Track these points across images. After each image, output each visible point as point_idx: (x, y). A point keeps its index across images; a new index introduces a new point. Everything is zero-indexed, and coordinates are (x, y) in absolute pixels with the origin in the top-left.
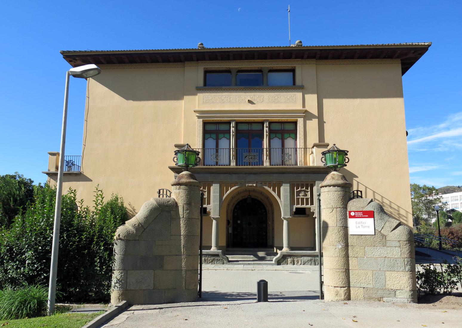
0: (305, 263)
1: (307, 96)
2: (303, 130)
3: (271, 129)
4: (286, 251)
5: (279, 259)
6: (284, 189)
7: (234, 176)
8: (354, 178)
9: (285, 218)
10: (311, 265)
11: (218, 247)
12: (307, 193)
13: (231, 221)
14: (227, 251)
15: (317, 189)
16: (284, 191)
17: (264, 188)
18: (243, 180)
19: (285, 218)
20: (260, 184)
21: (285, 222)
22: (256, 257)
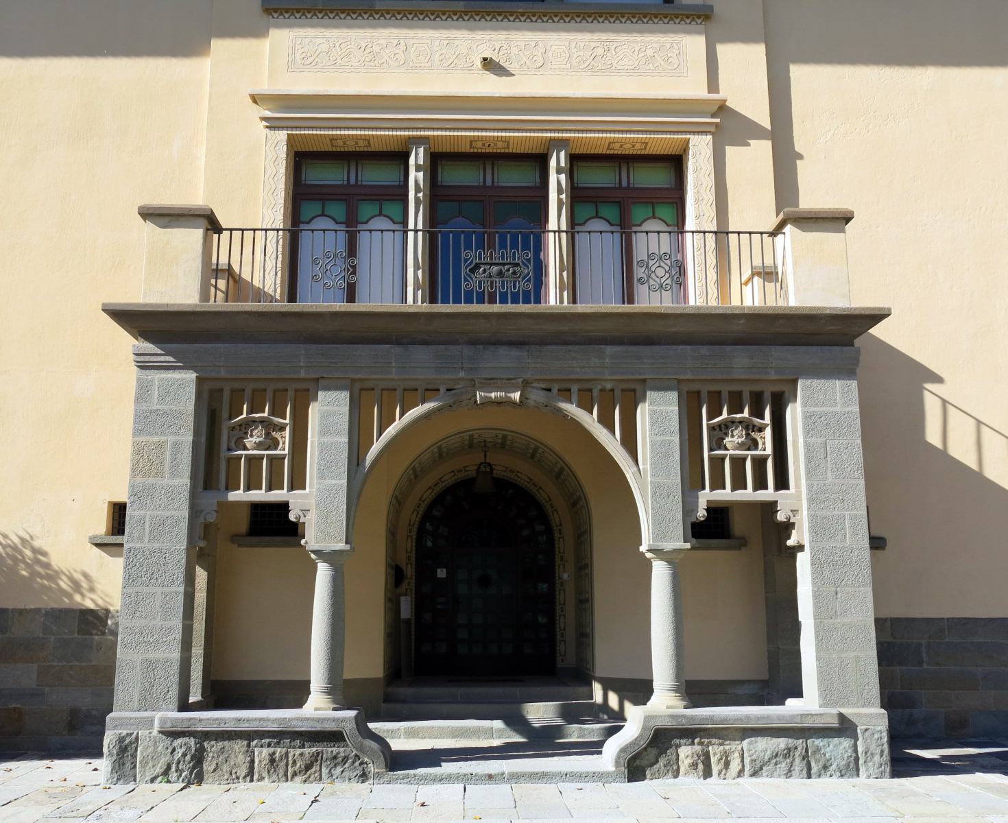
0: (761, 769)
1: (722, 50)
2: (710, 181)
3: (576, 185)
4: (668, 707)
5: (637, 749)
6: (652, 413)
7: (421, 354)
8: (928, 386)
9: (657, 552)
10: (788, 774)
11: (342, 692)
12: (755, 435)
13: (410, 571)
14: (388, 699)
15: (804, 413)
16: (652, 424)
17: (560, 410)
18: (462, 374)
19: (657, 552)
20: (543, 393)
21: (660, 574)
22: (520, 732)
